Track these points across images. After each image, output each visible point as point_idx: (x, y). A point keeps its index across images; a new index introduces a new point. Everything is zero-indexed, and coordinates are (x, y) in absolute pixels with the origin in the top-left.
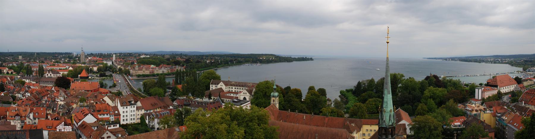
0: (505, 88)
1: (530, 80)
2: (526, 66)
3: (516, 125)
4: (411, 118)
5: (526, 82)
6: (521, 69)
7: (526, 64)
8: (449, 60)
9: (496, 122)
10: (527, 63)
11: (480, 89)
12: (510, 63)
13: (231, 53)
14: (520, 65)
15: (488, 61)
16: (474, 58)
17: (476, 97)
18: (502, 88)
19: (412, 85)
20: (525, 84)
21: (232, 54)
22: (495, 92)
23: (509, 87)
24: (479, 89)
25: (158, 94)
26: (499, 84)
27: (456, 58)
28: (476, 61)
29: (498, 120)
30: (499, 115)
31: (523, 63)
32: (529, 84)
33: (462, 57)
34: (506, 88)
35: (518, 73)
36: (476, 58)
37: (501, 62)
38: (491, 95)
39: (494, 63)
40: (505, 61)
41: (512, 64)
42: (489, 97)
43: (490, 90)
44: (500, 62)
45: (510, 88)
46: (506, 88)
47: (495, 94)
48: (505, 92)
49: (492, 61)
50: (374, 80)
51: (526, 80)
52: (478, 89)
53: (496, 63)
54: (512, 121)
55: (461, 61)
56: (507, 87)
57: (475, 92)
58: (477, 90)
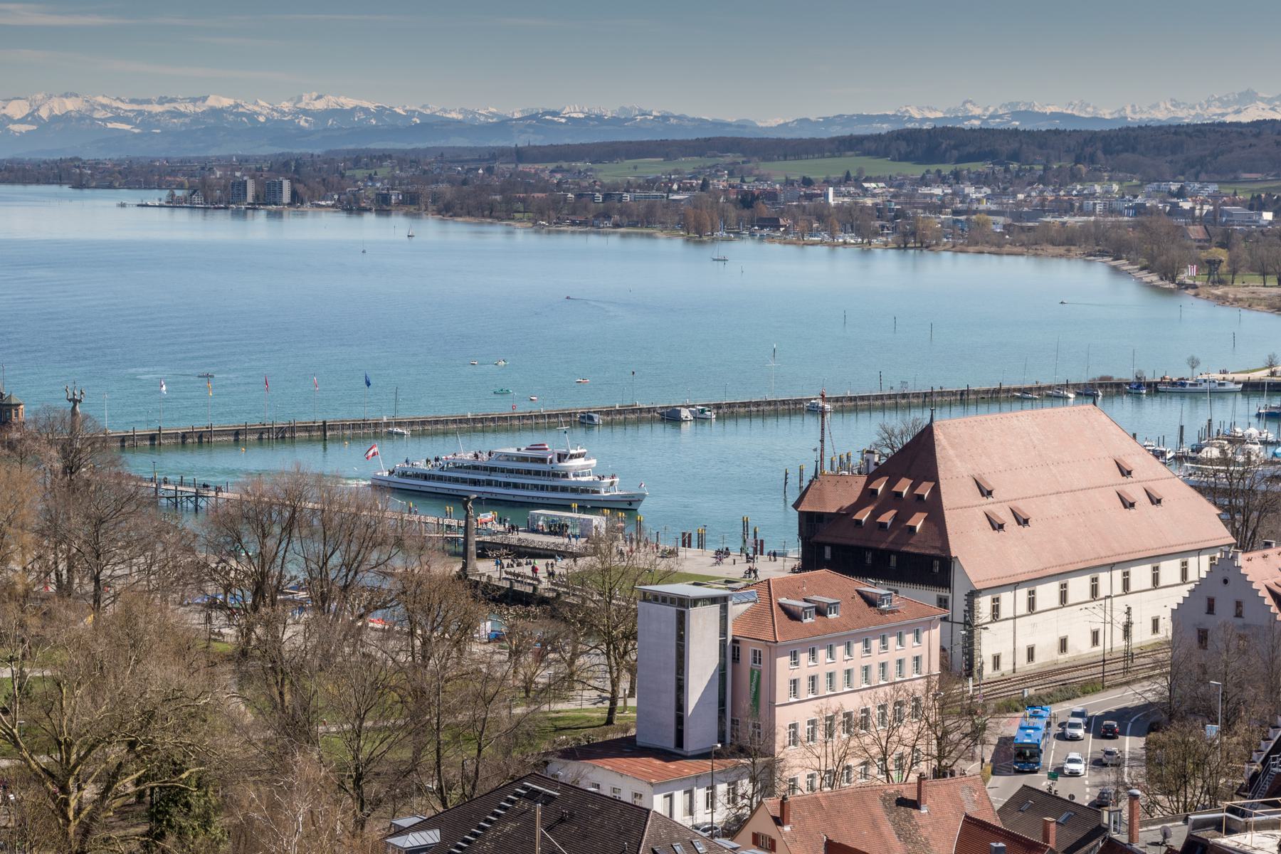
11: (695, 602)
24: (683, 604)
45: (1120, 604)
46: (1031, 604)
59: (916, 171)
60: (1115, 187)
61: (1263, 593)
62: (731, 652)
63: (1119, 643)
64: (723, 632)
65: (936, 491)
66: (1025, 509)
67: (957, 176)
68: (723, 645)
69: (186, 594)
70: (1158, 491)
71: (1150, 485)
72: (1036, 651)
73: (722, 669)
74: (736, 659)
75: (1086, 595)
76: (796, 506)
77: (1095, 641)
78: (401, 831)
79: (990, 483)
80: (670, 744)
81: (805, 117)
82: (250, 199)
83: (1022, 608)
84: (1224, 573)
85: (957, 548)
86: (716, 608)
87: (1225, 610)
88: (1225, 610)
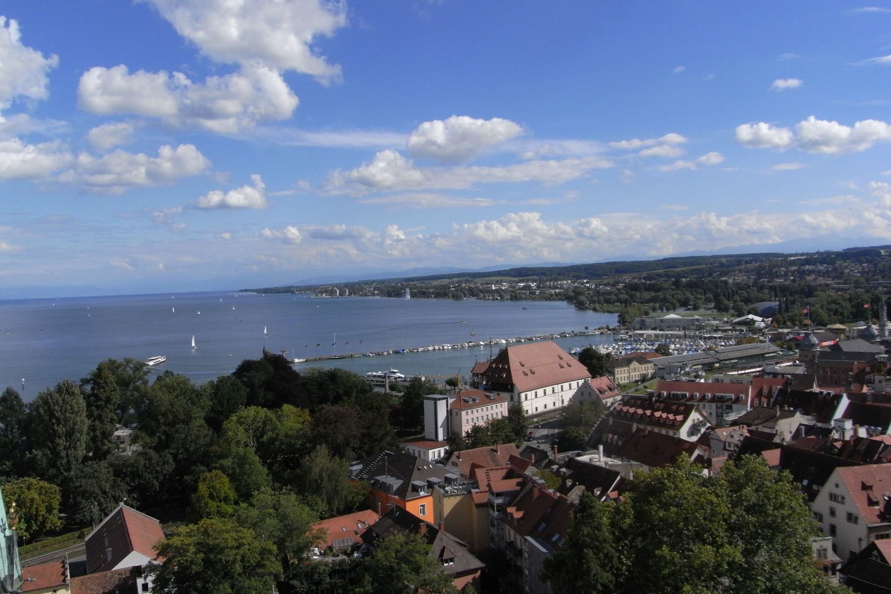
0: (540, 392)
1: (642, 359)
2: (633, 309)
3: (557, 541)
4: (163, 528)
5: (626, 369)
6: (612, 320)
7: (632, 297)
8: (341, 294)
9: (491, 529)
10: (638, 294)
11: (440, 399)
12: (572, 294)
13: (638, 260)
14: (608, 301)
15: (492, 292)
16: (435, 283)
17: (428, 432)
18: (531, 394)
19: (167, 477)
20: (623, 375)
21: (665, 259)
22: (500, 410)
23: (557, 388)
24: (436, 400)
25: (395, 238)
26: (517, 378)
27: (366, 283)
28: (442, 293)
29: (497, 519)
30: (499, 501)
31: (623, 296)
32: (636, 375)
33: (389, 281)
34: (545, 394)
35: (602, 333)
36: (445, 282)
37: (538, 292)
38: (481, 423)
39: (511, 299)
40: (555, 287)
41: (576, 299)
42: (476, 430)
43: (482, 404)
44: (534, 293)
45: (560, 394)
46: (545, 394)
47: (500, 417)
48: (541, 409)
49: (505, 291)
50: (17, 397)
51: (627, 361)
52: (433, 402)
53: (521, 299)
54: (544, 525)
55: (385, 296)
56: (549, 389)
57: (422, 413)
58: (428, 405)
59: (517, 279)
60: (569, 281)
61: (596, 390)
62: (450, 413)
63: (560, 405)
64: (447, 407)
65: (509, 367)
66: (534, 369)
67: (528, 281)
68: (447, 411)
69: (72, 446)
70: (570, 363)
71: (532, 369)
72: (547, 406)
73: (447, 417)
74: (451, 414)
75: (568, 388)
76: (471, 372)
77: (554, 405)
78: (352, 465)
79: (524, 363)
80: (434, 438)
81: (239, 363)
82: (347, 294)
83: (534, 396)
84: (586, 384)
85: (515, 380)
86: (445, 401)
87: (586, 396)
88: (586, 396)
